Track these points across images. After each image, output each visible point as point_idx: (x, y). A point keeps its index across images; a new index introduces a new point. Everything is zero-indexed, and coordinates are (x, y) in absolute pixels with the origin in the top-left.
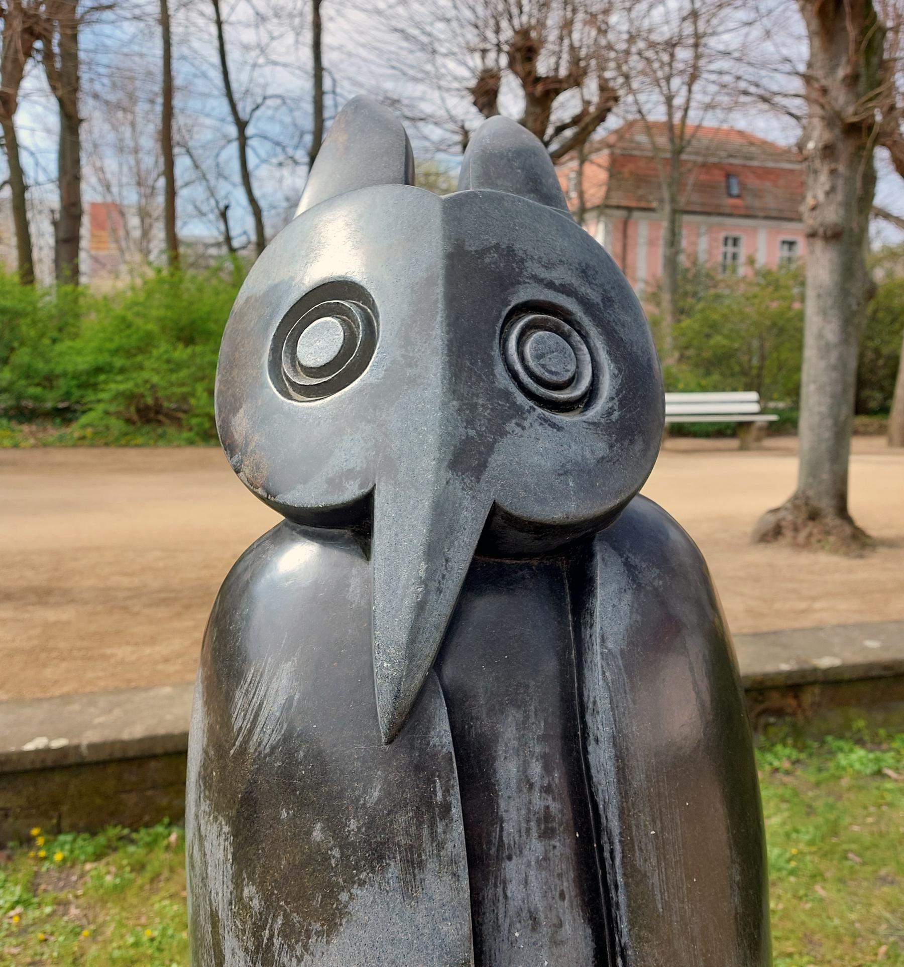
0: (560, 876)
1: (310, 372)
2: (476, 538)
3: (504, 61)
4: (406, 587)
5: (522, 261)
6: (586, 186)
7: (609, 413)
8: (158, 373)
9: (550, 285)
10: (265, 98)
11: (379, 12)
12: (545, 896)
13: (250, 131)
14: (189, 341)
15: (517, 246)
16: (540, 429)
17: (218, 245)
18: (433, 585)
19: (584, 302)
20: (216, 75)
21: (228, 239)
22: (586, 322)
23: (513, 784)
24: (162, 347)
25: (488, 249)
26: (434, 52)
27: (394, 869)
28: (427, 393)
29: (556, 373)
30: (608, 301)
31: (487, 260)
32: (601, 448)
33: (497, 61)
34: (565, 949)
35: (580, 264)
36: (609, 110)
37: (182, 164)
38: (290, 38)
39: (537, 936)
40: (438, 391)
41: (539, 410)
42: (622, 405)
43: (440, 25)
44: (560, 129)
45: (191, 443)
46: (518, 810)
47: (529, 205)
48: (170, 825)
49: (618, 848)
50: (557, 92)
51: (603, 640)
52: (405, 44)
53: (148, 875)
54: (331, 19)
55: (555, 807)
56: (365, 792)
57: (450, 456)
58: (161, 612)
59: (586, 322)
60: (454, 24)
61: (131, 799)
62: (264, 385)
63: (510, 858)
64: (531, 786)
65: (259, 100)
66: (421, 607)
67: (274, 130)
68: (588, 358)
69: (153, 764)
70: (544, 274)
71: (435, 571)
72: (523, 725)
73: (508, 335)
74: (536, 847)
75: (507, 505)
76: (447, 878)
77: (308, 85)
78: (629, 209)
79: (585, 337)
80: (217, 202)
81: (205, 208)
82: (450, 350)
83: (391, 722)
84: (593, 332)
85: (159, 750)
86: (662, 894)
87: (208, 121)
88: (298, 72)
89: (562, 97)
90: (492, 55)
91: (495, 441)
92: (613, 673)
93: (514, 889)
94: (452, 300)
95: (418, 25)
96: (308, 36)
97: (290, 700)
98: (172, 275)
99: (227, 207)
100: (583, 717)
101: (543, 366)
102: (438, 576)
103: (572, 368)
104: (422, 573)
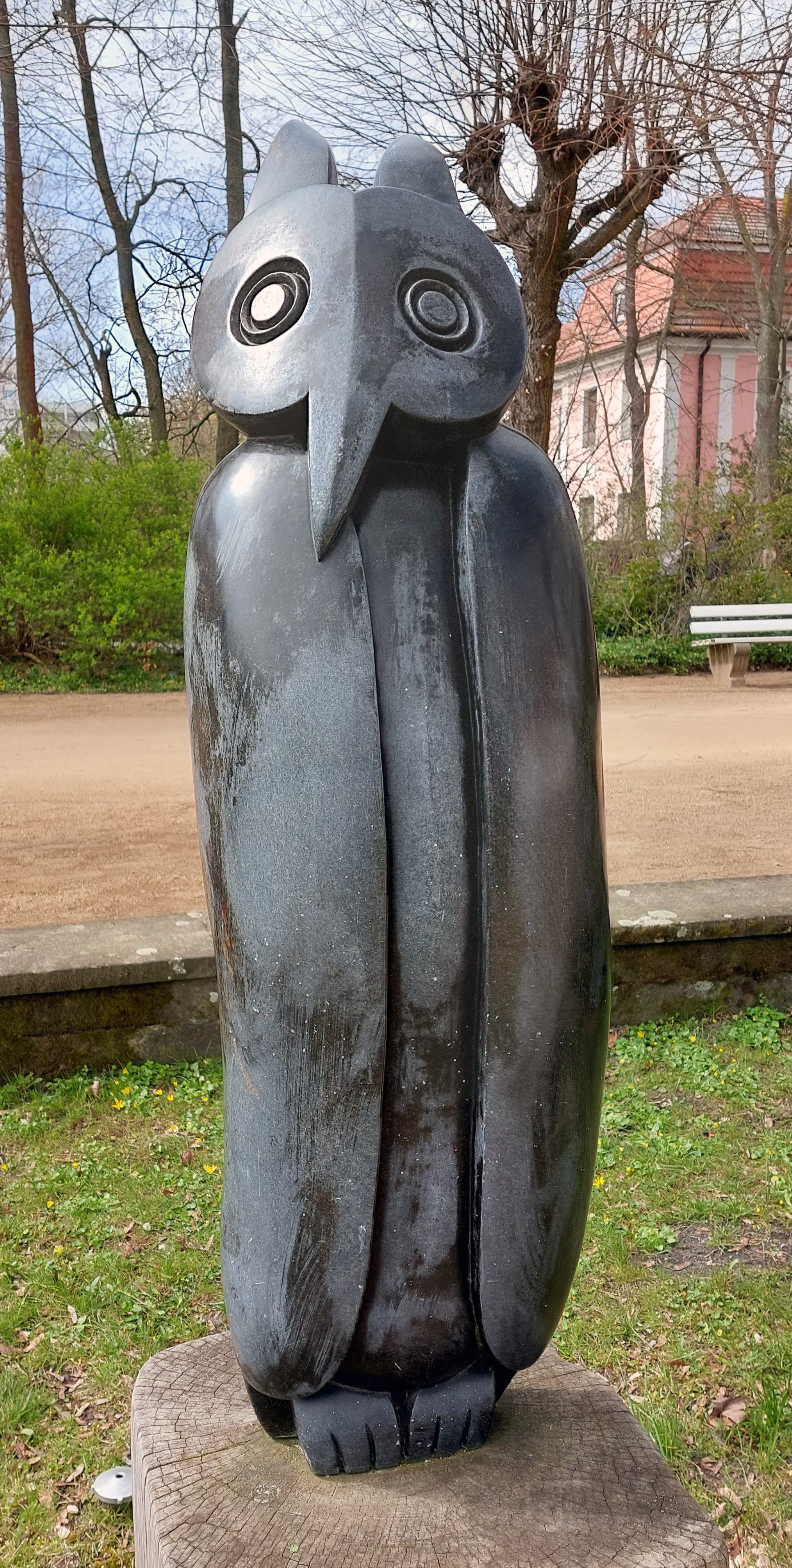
0: (437, 658)
1: (260, 325)
2: (378, 427)
3: (506, 108)
4: (330, 454)
5: (417, 240)
6: (640, 300)
7: (481, 352)
8: (23, 590)
9: (439, 258)
10: (155, 185)
11: (322, 43)
12: (426, 667)
13: (136, 235)
14: (63, 545)
15: (412, 230)
16: (427, 358)
17: (93, 414)
18: (349, 453)
19: (469, 276)
20: (82, 150)
21: (110, 402)
22: (466, 286)
23: (406, 598)
24: (30, 551)
25: (389, 232)
26: (405, 99)
27: (325, 635)
28: (343, 329)
29: (441, 321)
30: (485, 273)
31: (389, 239)
32: (473, 375)
33: (496, 109)
34: (441, 701)
35: (464, 244)
36: (664, 179)
37: (40, 288)
38: (190, 90)
39: (420, 691)
40: (351, 327)
41: (426, 345)
42: (491, 347)
43: (412, 59)
44: (592, 211)
45: (74, 688)
46: (409, 615)
47: (423, 200)
48: (90, 1074)
49: (476, 637)
50: (585, 153)
51: (470, 506)
52: (360, 90)
53: (68, 1121)
54: (251, 56)
55: (434, 616)
56: (306, 590)
57: (358, 372)
58: (60, 863)
59: (466, 286)
60: (433, 56)
61: (43, 1043)
62: (227, 339)
63: (402, 644)
64: (418, 601)
65: (148, 190)
66: (340, 466)
67: (171, 232)
68: (466, 312)
69: (67, 1003)
70: (434, 250)
71: (350, 445)
72: (412, 564)
73: (404, 295)
74: (420, 639)
75: (400, 405)
76: (359, 641)
77: (219, 162)
78: (708, 338)
79: (466, 300)
80: (91, 347)
81: (75, 357)
82: (360, 298)
83: (322, 542)
84: (472, 294)
85: (75, 987)
86: (506, 671)
87: (72, 223)
88: (202, 141)
89: (593, 164)
90: (490, 101)
91: (393, 363)
92: (476, 527)
93: (405, 662)
94: (361, 265)
95: (379, 61)
96: (216, 86)
97: (256, 539)
98: (36, 451)
99: (106, 353)
100: (456, 560)
101: (431, 315)
102: (352, 448)
103: (453, 318)
104: (341, 444)
